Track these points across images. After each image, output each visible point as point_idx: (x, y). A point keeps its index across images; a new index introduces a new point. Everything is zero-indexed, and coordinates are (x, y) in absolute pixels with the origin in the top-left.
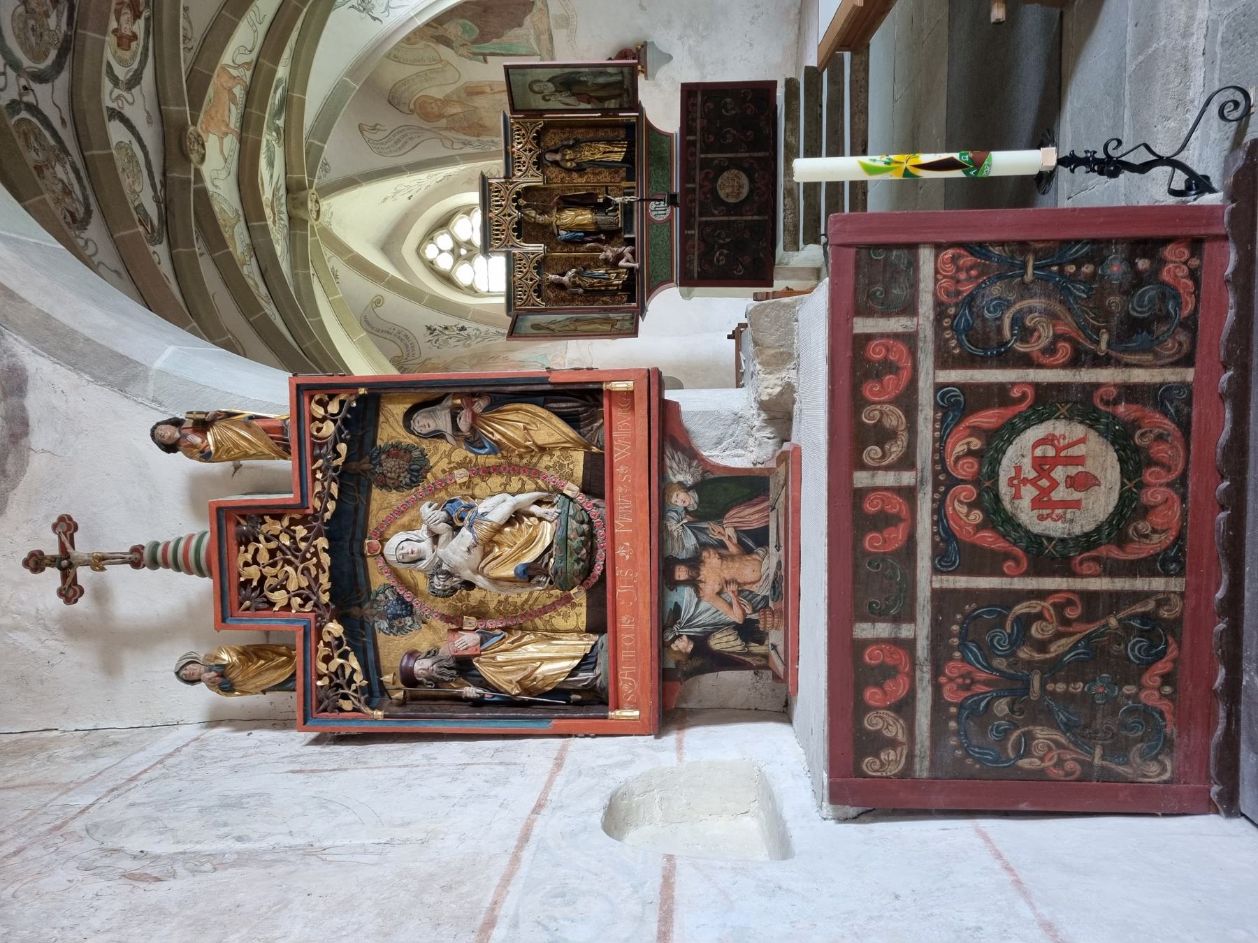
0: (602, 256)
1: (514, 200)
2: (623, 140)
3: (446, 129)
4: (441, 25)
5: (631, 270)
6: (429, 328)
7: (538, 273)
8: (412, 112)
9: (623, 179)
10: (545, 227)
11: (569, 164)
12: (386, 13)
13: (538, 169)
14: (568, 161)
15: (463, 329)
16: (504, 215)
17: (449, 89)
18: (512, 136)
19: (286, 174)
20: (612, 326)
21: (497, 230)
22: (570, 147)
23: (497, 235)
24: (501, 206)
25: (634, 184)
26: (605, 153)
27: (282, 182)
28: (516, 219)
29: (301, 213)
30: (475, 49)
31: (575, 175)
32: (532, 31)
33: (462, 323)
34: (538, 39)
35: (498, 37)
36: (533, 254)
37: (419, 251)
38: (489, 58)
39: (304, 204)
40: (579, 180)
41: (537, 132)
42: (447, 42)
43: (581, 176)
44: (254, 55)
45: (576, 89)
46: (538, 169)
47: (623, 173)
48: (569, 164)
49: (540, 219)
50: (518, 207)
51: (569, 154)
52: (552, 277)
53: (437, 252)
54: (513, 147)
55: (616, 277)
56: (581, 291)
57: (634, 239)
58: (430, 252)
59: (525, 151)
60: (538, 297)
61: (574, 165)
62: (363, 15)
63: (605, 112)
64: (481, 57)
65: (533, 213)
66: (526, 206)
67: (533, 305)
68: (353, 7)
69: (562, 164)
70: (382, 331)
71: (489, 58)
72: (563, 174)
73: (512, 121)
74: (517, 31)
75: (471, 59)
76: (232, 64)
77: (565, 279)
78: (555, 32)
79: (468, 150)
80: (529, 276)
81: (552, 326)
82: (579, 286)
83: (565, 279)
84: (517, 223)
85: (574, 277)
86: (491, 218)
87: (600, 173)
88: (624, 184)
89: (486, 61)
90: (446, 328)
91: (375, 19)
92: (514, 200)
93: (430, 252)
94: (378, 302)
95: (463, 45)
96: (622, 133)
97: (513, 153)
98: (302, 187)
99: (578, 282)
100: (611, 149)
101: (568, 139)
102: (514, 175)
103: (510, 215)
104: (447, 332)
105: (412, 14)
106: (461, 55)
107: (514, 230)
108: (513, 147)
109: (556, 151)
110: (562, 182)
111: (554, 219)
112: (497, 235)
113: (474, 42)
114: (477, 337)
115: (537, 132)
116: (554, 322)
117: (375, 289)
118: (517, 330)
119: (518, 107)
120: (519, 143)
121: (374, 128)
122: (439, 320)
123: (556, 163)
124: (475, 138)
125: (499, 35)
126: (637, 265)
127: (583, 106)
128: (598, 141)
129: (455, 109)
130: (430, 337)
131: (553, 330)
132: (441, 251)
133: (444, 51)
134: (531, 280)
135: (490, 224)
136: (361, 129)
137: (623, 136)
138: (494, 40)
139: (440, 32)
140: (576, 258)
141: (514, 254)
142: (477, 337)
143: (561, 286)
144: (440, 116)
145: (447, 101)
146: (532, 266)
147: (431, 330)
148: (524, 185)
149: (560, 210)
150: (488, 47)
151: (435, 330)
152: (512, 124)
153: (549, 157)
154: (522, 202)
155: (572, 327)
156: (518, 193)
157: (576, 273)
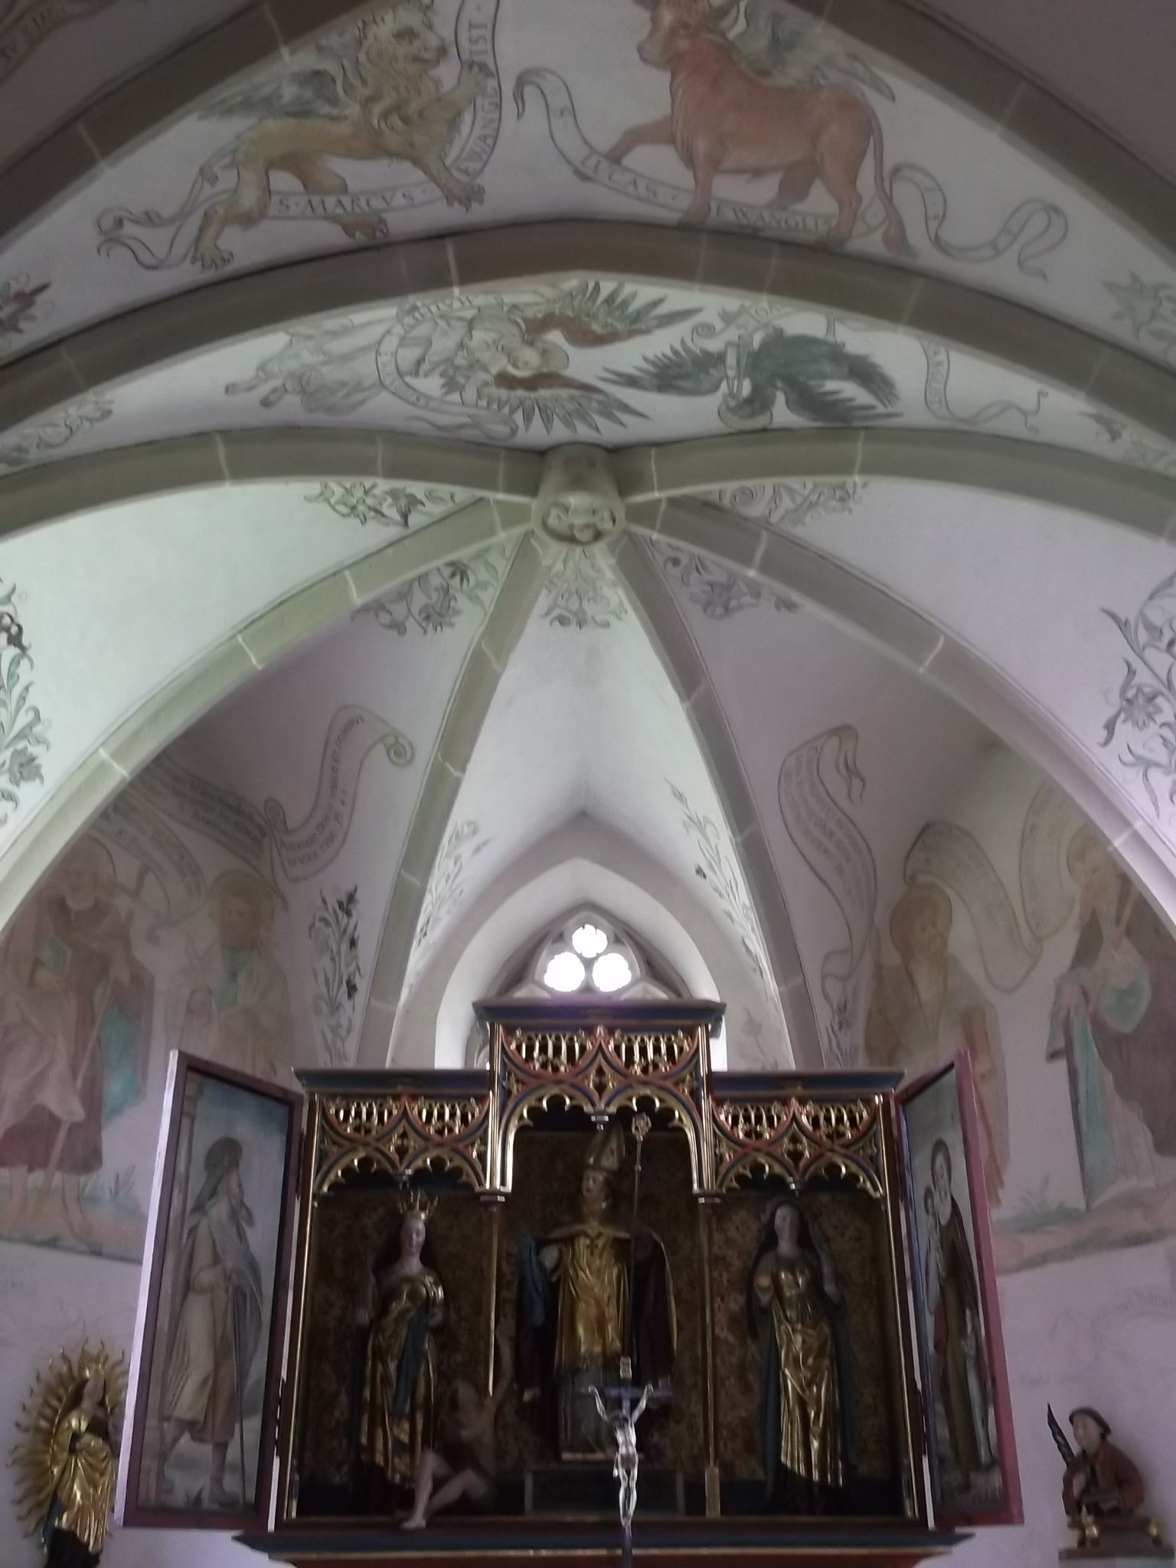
0: (465, 1392)
1: (645, 1103)
2: (849, 1470)
3: (879, 968)
4: (1128, 932)
5: (407, 1500)
6: (351, 898)
7: (420, 1172)
8: (910, 880)
9: (726, 1468)
10: (573, 1203)
11: (764, 1281)
12: (1129, 758)
13: (740, 1178)
14: (775, 1279)
15: (352, 989)
16: (600, 1072)
17: (972, 967)
18: (833, 1101)
19: (659, 444)
20: (189, 1426)
21: (557, 1050)
22: (816, 1282)
23: (544, 1049)
24: (630, 1061)
25: (713, 1510)
26: (803, 1405)
27: (633, 430)
28: (588, 1108)
29: (553, 479)
30: (1082, 1029)
31: (736, 1303)
32: (1149, 1183)
33: (363, 985)
34: (1133, 1201)
35: (1120, 1088)
36: (482, 1157)
37: (588, 910)
38: (1062, 1065)
39: (578, 483)
40: (721, 1317)
41: (852, 1177)
42: (1087, 950)
43: (733, 1321)
44: (929, 258)
45: (21, 702)
46: (740, 1178)
47: (750, 1469)
48: (764, 1281)
49: (594, 1183)
50: (624, 1116)
51: (793, 1283)
52: (419, 1222)
53: (589, 954)
54: (803, 1102)
55: (397, 1442)
56: (364, 1316)
57: (519, 1509)
58: (589, 939)
59: (794, 1140)
60: (348, 1171)
61: (765, 1299)
62: (1115, 698)
63: (920, 1409)
64: (1061, 1043)
65: (610, 1162)
66: (631, 1142)
67: (322, 1156)
68: (1131, 672)
69: (767, 1260)
70: (334, 770)
71: (1062, 1065)
72: (737, 1264)
73: (878, 1100)
74: (1143, 1139)
75: (1053, 1016)
76: (889, 164)
77: (413, 1265)
78: (1157, 1251)
79: (824, 1017)
80: (413, 1143)
81: (219, 1210)
82: (383, 1309)
83: (413, 1265)
84: (577, 1109)
85: (413, 1295)
86: (590, 1031)
87: (746, 1387)
88: (712, 1475)
89: (1053, 1056)
90: (353, 943)
91: (1110, 727)
92: (645, 1103)
93: (589, 939)
94: (399, 751)
95: (1085, 994)
96: (869, 1467)
97: (785, 1102)
98: (625, 486)
99: (396, 1308)
100: (817, 1427)
101: (839, 1279)
102: (719, 1103)
103: (601, 1088)
104: (345, 946)
105: (1138, 825)
106: (1059, 992)
107: (556, 1102)
108: (803, 1102)
109: (803, 1239)
110: (718, 1261)
111: (593, 1227)
112: (544, 1049)
113: (1098, 1024)
114: (335, 1030)
115: (852, 1177)
116: (240, 1215)
117: (425, 736)
118: (212, 1089)
119: (281, 1111)
120: (815, 1122)
121: (851, 771)
122: (370, 920)
123: (769, 1240)
124: (860, 1039)
125: (1125, 1087)
126: (418, 1520)
127: (930, 1322)
128: (841, 1381)
129: (927, 988)
130: (332, 903)
131: (200, 1208)
132: (588, 964)
133: (1063, 948)
134: (402, 1151)
135: (575, 1029)
136: (842, 731)
137: (863, 1469)
138: (1109, 1078)
139: (1110, 931)
140: (479, 1307)
141: (482, 1100)
142: (335, 1030)
143: (393, 1251)
144: (907, 949)
145: (944, 963)
146: (444, 1153)
147: (348, 904)
148: (691, 1135)
149: (620, 1249)
150: (1089, 1057)
151: (349, 914)
152: (868, 1102)
153: (784, 1218)
154: (641, 1127)
155: (205, 1277)
156: (668, 1113)
157: (429, 1302)
